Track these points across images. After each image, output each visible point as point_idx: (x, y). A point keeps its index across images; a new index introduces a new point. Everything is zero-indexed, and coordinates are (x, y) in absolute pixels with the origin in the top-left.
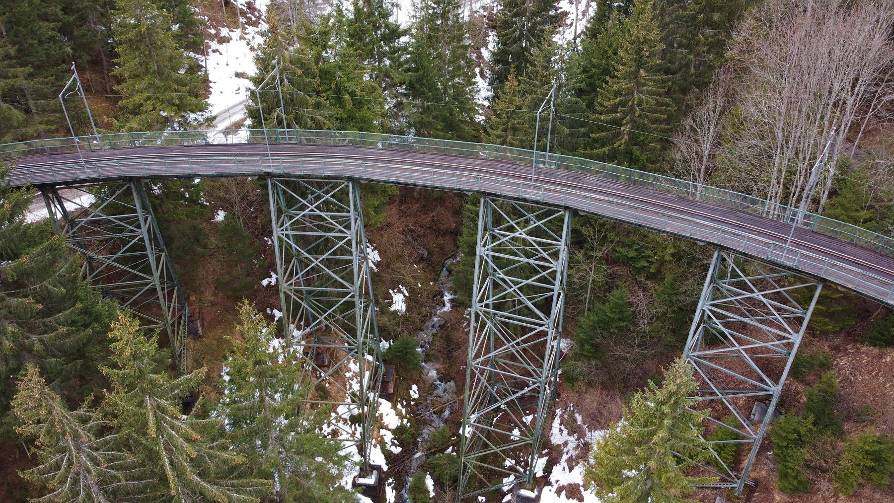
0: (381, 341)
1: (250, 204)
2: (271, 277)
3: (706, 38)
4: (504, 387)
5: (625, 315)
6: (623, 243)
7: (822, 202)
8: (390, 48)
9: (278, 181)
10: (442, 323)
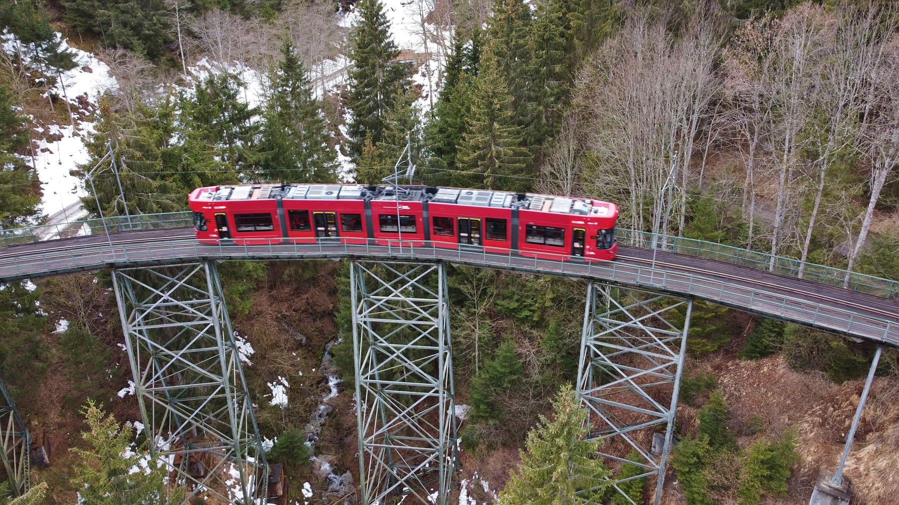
0: (264, 441)
1: (97, 307)
2: (128, 386)
3: (552, 89)
4: (404, 466)
5: (516, 368)
6: (503, 296)
7: (681, 228)
8: (241, 128)
9: (124, 272)
10: (330, 411)
